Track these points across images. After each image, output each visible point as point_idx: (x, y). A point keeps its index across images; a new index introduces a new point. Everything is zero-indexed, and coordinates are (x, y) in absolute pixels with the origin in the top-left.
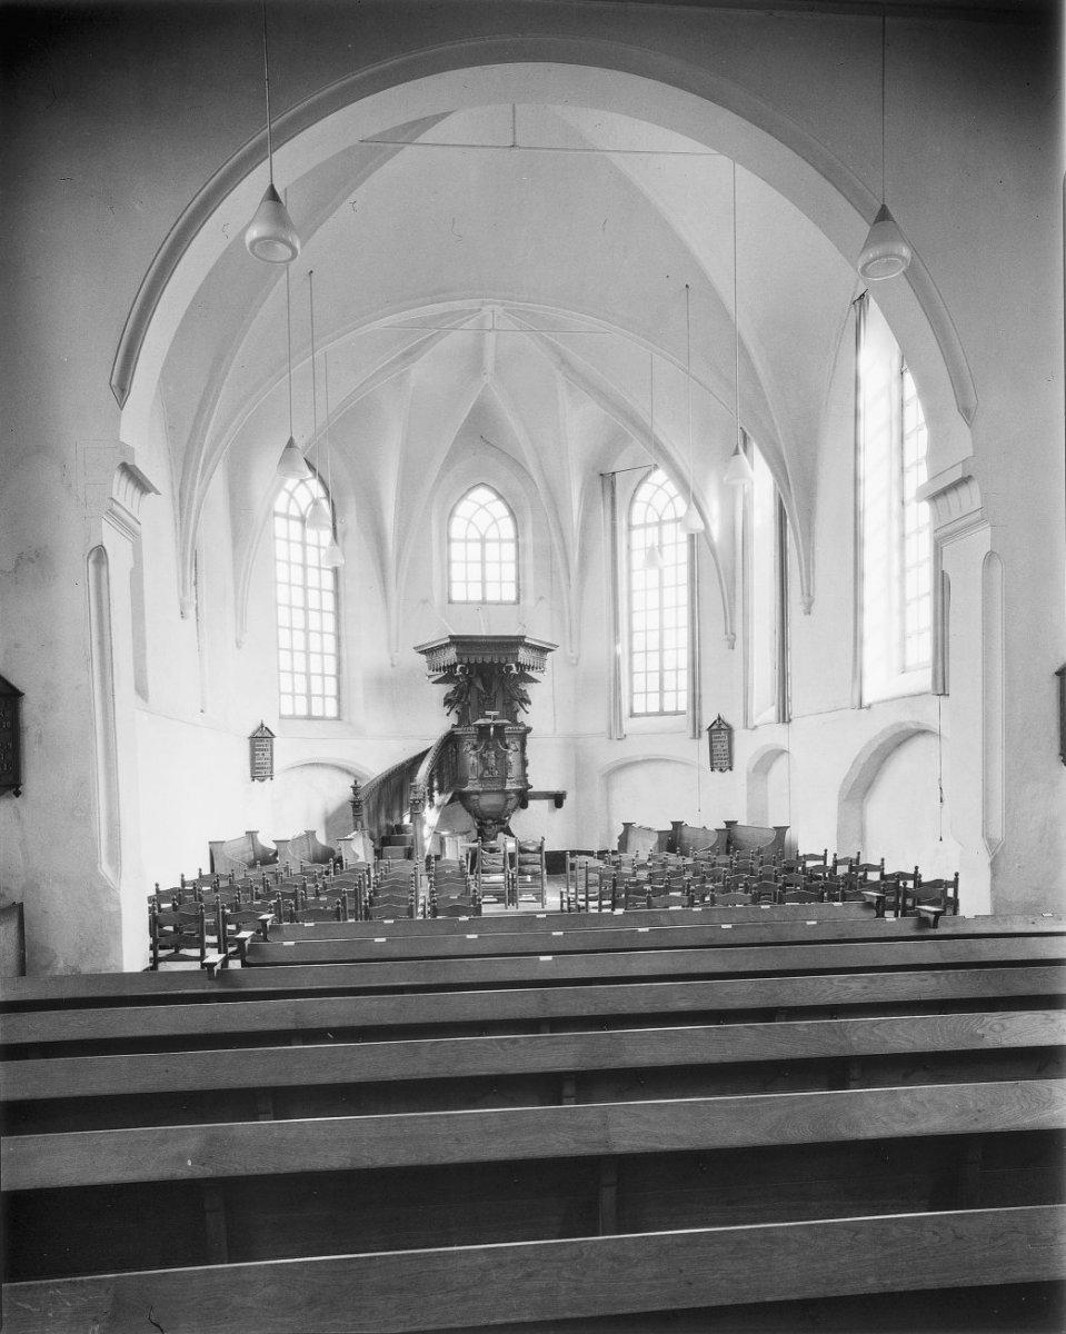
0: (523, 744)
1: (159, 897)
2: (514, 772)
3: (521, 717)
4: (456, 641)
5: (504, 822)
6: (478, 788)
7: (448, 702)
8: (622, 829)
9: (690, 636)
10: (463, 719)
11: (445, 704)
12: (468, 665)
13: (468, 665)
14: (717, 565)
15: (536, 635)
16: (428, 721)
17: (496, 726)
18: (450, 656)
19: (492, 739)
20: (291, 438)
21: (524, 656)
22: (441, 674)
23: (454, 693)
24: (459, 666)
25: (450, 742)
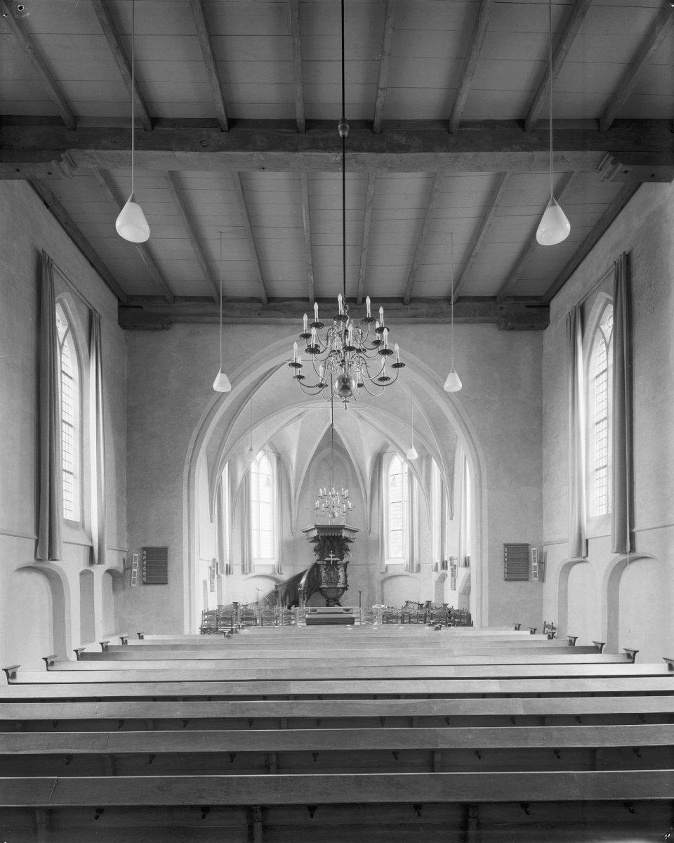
0: (346, 568)
2: (342, 580)
6: (326, 586)
10: (322, 558)
16: (306, 559)
17: (333, 561)
18: (315, 533)
21: (345, 534)
22: (311, 540)
25: (316, 567)
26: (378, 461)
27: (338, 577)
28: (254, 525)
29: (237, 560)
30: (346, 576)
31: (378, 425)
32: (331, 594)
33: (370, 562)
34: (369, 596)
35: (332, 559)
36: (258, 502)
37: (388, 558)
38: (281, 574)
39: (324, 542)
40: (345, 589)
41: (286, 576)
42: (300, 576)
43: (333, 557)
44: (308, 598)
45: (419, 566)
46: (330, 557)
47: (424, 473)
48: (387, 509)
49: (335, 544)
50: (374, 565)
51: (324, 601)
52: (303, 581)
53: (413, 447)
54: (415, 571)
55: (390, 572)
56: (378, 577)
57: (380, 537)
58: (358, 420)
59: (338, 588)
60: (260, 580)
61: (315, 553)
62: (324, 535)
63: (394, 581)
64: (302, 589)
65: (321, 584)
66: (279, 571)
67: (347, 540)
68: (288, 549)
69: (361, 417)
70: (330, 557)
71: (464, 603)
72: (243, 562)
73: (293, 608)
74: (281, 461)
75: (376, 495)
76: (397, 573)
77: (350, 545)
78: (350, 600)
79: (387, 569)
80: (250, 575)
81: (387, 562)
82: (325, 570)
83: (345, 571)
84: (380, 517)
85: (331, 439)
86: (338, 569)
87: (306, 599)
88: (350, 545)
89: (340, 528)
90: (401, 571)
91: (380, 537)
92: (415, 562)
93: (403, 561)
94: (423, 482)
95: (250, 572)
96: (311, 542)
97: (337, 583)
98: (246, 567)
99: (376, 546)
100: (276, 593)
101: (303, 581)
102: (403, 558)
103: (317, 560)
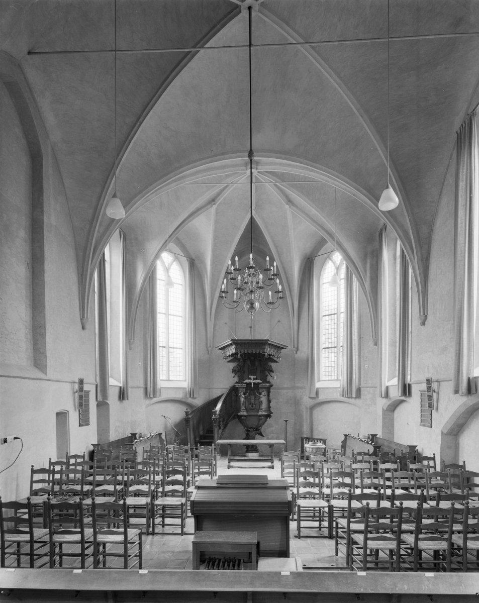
0: (269, 392)
1: (267, 476)
2: (264, 406)
3: (269, 378)
4: (236, 343)
5: (259, 430)
6: (245, 413)
7: (234, 371)
8: (343, 437)
9: (125, 368)
10: (241, 381)
11: (233, 372)
12: (244, 353)
13: (244, 353)
14: (206, 335)
15: (275, 340)
16: (224, 380)
17: (254, 383)
18: (232, 350)
19: (253, 390)
20: (252, 218)
21: (268, 351)
22: (230, 358)
23: (237, 367)
24: (240, 354)
25: (234, 391)
26: (309, 267)
27: (260, 403)
28: (161, 339)
29: (138, 380)
30: (269, 401)
31: (314, 211)
32: (253, 422)
33: (297, 385)
34: (295, 424)
35: (252, 381)
36: (167, 314)
37: (319, 381)
38: (193, 398)
39: (244, 361)
40: (269, 416)
41: (199, 401)
42: (216, 401)
43: (254, 379)
44: (225, 427)
45: (359, 390)
46: (250, 379)
47: (368, 274)
48: (319, 324)
49: (257, 363)
50: (301, 388)
51: (241, 429)
52: (219, 407)
53: (390, 186)
54: (354, 396)
55: (322, 397)
56: (307, 401)
57: (310, 359)
58: (287, 206)
59: (260, 416)
60: (169, 405)
61: (233, 375)
62: (243, 351)
63: (325, 407)
64: (217, 416)
65: (239, 411)
66: (191, 394)
67: (271, 359)
68: (201, 368)
69: (290, 201)
70: (250, 379)
71: (449, 448)
72: (146, 383)
73: (201, 449)
74: (194, 267)
75: (306, 305)
76: (330, 398)
77: (273, 365)
78: (274, 429)
79: (317, 393)
80: (155, 400)
81: (318, 385)
82: (244, 394)
83: (269, 395)
84: (310, 332)
85: (253, 240)
86: (260, 394)
87: (222, 427)
88: (273, 365)
89: (263, 343)
90: (337, 396)
91: (310, 359)
92: (112, 382)
93: (338, 384)
94: (367, 284)
95: (154, 397)
96: (229, 362)
97: (259, 409)
98: (150, 390)
99: (307, 367)
100: (186, 421)
101: (219, 407)
102: (337, 380)
103: (237, 383)
